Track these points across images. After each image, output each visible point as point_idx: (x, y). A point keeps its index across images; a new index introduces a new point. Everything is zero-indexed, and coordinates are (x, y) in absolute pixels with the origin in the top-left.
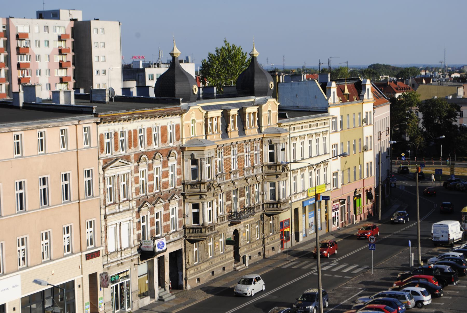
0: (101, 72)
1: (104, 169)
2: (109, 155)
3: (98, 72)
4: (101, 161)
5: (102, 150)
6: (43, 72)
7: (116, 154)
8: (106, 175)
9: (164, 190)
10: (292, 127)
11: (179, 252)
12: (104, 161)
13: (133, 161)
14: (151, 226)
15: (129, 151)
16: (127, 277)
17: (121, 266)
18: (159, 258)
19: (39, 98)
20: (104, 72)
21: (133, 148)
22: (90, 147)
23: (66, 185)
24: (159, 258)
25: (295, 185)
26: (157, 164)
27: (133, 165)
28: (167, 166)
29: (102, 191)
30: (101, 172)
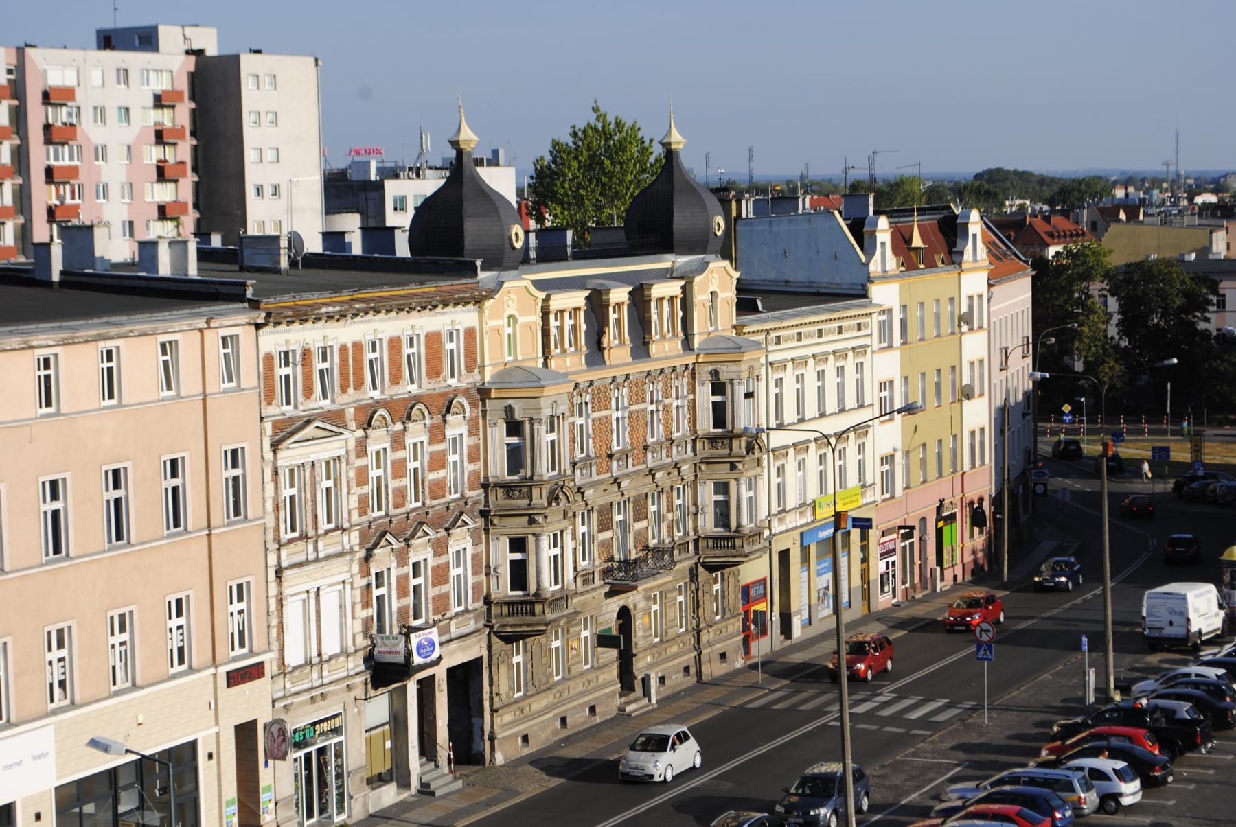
0: (268, 191)
1: (275, 446)
2: (288, 410)
3: (259, 190)
4: (268, 426)
5: (269, 397)
6: (114, 191)
7: (306, 406)
8: (280, 463)
9: (435, 502)
10: (773, 335)
11: (475, 665)
12: (275, 425)
13: (353, 425)
14: (399, 598)
15: (342, 399)
16: (336, 731)
17: (321, 703)
18: (420, 682)
19: (102, 258)
20: (276, 191)
21: (351, 390)
22: (239, 388)
23: (175, 489)
24: (420, 682)
25: (781, 489)
26: (417, 433)
27: (352, 436)
28: (443, 440)
29: (269, 506)
30: (269, 455)
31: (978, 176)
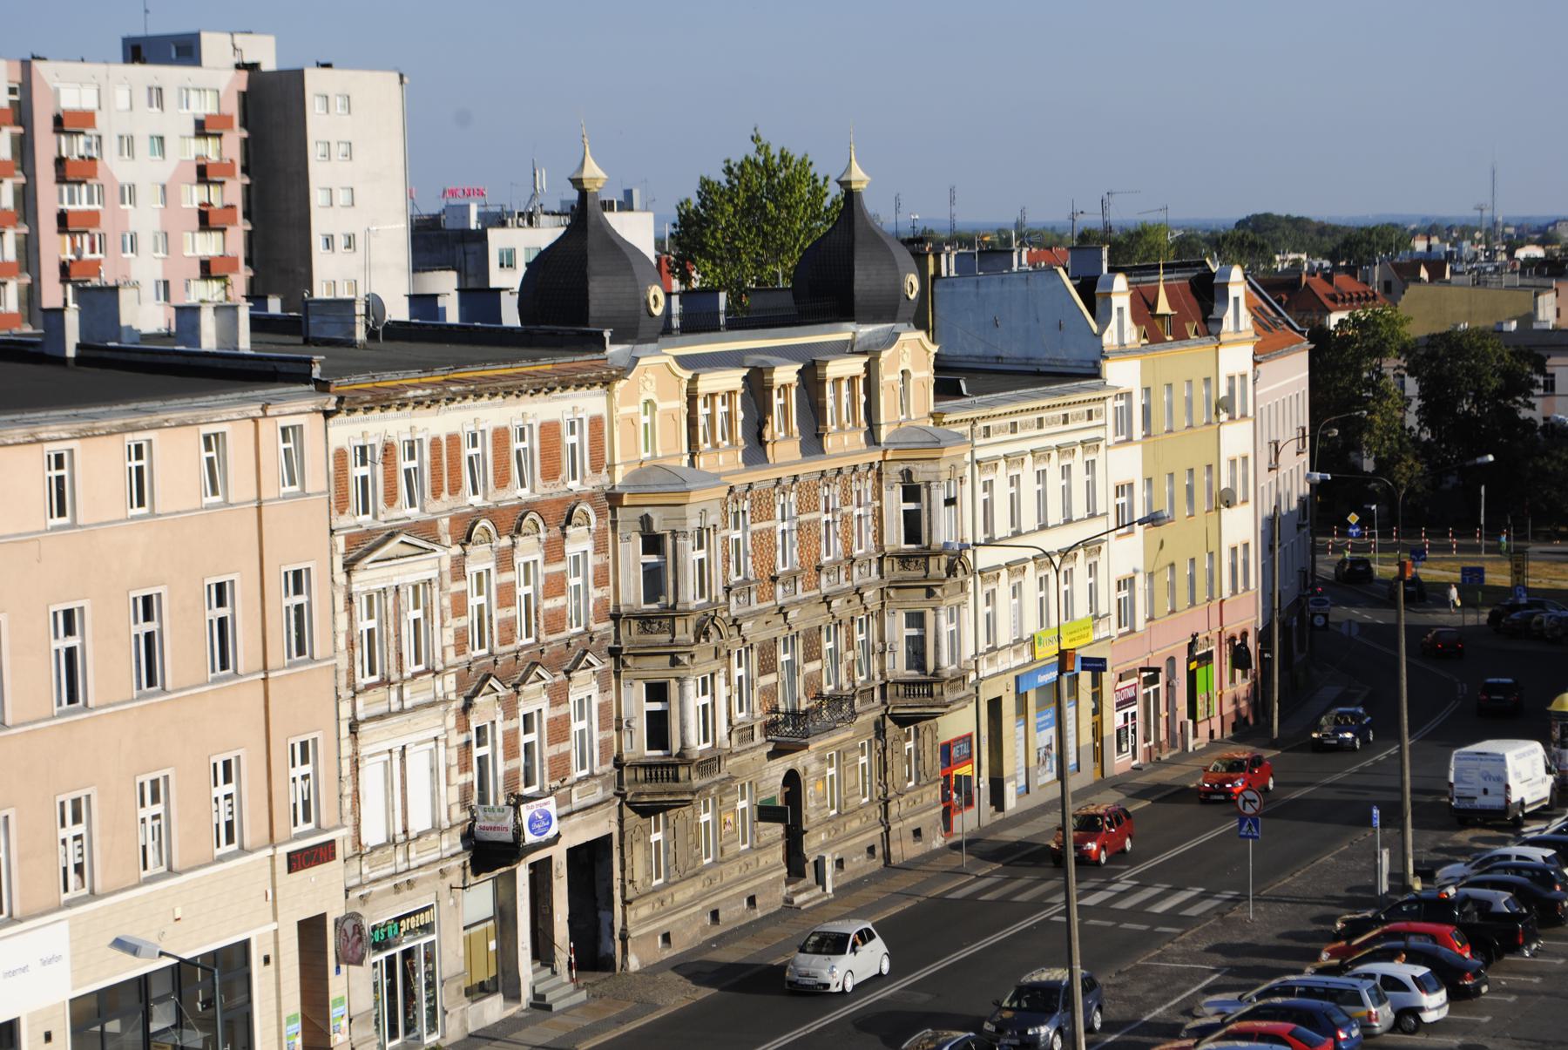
0: (340, 242)
1: (349, 567)
2: (366, 520)
3: (329, 242)
4: (340, 541)
5: (341, 504)
6: (145, 243)
7: (388, 516)
8: (355, 588)
9: (552, 638)
10: (981, 425)
11: (602, 845)
12: (349, 540)
13: (447, 540)
15: (434, 506)
16: (427, 928)
17: (407, 893)
18: (532, 866)
19: (130, 328)
20: (350, 242)
21: (445, 496)
22: (303, 493)
23: (222, 621)
24: (532, 866)
25: (991, 620)
26: (529, 549)
27: (446, 554)
28: (562, 558)
29: (342, 642)
30: (341, 578)
31: (1241, 224)
